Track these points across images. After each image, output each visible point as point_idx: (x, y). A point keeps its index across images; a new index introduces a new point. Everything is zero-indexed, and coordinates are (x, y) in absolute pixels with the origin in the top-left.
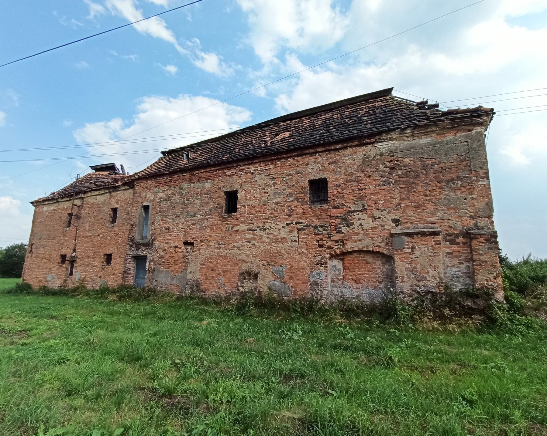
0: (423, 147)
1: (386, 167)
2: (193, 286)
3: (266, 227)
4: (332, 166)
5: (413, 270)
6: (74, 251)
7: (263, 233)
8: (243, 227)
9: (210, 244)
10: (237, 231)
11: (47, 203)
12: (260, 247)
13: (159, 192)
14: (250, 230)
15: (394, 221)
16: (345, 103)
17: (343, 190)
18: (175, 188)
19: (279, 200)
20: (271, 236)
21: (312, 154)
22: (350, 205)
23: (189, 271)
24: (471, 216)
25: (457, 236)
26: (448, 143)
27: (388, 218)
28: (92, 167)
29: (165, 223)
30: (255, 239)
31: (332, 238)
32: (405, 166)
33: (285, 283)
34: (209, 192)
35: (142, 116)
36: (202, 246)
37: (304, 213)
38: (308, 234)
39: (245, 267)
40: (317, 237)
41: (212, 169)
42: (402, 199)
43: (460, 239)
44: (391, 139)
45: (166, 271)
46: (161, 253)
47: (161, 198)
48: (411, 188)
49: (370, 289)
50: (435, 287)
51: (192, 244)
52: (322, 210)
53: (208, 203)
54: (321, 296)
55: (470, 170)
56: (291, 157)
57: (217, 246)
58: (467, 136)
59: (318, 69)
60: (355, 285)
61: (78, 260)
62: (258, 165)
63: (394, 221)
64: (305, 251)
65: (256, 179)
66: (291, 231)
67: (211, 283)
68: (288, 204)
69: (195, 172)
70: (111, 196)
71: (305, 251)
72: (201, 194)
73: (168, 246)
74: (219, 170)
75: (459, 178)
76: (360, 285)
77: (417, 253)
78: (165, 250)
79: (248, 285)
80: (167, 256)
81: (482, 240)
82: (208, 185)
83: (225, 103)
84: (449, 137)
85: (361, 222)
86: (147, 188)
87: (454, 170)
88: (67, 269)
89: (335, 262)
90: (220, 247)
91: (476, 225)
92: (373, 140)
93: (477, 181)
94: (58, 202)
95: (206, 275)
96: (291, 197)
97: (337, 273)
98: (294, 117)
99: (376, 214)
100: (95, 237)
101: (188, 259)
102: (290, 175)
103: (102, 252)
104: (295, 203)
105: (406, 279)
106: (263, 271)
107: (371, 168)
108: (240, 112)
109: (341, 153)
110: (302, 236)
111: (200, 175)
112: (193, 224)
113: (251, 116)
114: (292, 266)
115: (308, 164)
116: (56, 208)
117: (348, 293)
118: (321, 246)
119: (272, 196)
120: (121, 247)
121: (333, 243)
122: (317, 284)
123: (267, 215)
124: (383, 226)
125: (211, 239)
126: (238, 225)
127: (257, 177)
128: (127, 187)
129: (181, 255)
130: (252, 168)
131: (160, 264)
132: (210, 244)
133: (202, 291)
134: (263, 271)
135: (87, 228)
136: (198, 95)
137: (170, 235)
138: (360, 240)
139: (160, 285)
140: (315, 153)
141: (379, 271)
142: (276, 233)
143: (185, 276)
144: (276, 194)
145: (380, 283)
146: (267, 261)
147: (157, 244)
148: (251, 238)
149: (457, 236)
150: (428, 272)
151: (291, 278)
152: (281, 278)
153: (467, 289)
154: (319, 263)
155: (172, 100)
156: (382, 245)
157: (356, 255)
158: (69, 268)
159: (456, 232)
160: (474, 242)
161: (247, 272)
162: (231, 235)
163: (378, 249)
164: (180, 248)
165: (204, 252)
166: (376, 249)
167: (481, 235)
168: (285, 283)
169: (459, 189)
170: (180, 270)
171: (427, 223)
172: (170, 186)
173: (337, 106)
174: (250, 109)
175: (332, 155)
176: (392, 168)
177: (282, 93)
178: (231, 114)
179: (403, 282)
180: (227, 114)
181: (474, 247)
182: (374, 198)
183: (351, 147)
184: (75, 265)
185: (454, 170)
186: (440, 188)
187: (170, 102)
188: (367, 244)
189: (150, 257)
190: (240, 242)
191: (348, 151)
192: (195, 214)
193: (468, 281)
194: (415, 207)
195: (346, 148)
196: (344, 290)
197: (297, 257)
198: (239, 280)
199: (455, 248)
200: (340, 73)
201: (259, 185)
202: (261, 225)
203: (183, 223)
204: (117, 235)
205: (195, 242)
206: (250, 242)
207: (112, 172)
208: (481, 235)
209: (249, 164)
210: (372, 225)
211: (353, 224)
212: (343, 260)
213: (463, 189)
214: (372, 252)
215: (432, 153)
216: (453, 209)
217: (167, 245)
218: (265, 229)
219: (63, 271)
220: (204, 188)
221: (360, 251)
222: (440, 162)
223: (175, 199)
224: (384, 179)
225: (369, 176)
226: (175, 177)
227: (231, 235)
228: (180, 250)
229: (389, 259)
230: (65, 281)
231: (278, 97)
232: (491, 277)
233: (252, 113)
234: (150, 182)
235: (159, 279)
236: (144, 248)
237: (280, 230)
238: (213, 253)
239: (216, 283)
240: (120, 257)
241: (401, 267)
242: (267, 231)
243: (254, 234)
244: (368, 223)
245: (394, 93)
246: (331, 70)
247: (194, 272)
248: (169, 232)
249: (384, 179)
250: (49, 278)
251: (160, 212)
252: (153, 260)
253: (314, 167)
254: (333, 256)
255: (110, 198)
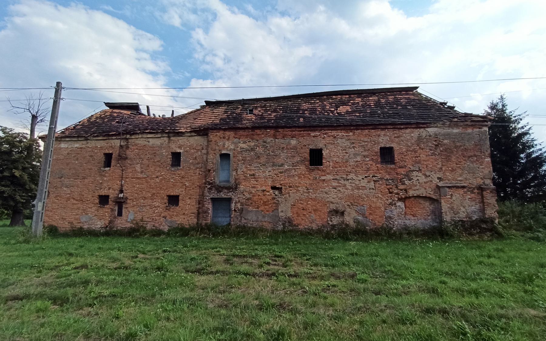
0: (456, 134)
1: (433, 144)
2: (286, 222)
3: (348, 178)
4: (397, 139)
5: (452, 208)
6: (121, 191)
7: (346, 182)
8: (329, 177)
9: (299, 189)
10: (324, 180)
11: (67, 139)
12: (345, 192)
13: (240, 143)
14: (336, 179)
15: (438, 178)
16: (385, 91)
17: (405, 156)
18: (257, 140)
19: (359, 159)
20: (354, 185)
21: (382, 129)
22: (411, 167)
23: (280, 210)
24: (481, 178)
25: (474, 189)
26: (469, 134)
27: (434, 177)
28: (107, 104)
29: (250, 170)
30: (340, 187)
31: (399, 188)
32: (445, 145)
33: (366, 217)
34: (295, 148)
35: (18, 20)
36: (291, 190)
37: (378, 170)
38: (381, 184)
39: (333, 207)
40: (388, 187)
41: (298, 129)
42: (442, 165)
43: (476, 191)
44: (436, 127)
45: (256, 211)
46: (248, 196)
47: (243, 148)
48: (448, 159)
49: (423, 220)
50: (464, 218)
51: (280, 189)
52: (391, 168)
53: (294, 156)
54: (394, 225)
55: (481, 152)
56: (366, 129)
57: (306, 191)
58: (479, 131)
59: (236, 10)
60: (413, 218)
61: (128, 201)
62: (339, 131)
63: (438, 178)
64: (380, 196)
65: (338, 141)
66: (369, 182)
67: (303, 220)
68: (366, 163)
69: (280, 130)
70: (169, 140)
71: (380, 196)
72: (287, 149)
73: (255, 189)
74: (304, 131)
75: (475, 156)
76: (416, 218)
77: (454, 198)
78: (251, 193)
79: (336, 220)
80: (255, 198)
81: (488, 191)
82: (294, 142)
83: (132, 27)
84: (470, 130)
85: (418, 178)
86: (224, 138)
87: (472, 151)
88: (112, 210)
89: (399, 204)
90: (309, 192)
91: (484, 183)
92: (425, 126)
93: (485, 158)
94: (87, 139)
95: (297, 213)
96: (367, 157)
97: (401, 210)
98: (344, 93)
99: (428, 174)
100: (153, 178)
101: (278, 201)
102: (366, 142)
103: (164, 194)
104: (371, 162)
105: (448, 213)
106: (348, 210)
107: (423, 144)
108: (150, 39)
109: (403, 131)
110: (377, 185)
111: (284, 132)
112: (281, 173)
113: (162, 46)
114: (371, 206)
115: (379, 136)
116: (84, 146)
117: (408, 222)
118: (390, 193)
119: (352, 156)
120: (190, 190)
121: (399, 191)
122: (390, 217)
123: (349, 169)
124: (431, 181)
125: (300, 185)
126: (325, 175)
127: (339, 141)
128: (193, 134)
129: (270, 198)
130: (334, 133)
131: (248, 205)
132: (299, 189)
133: (295, 225)
134: (348, 210)
135: (139, 170)
136: (98, 9)
137: (257, 181)
138: (417, 190)
139: (251, 222)
140: (385, 129)
141: (428, 209)
142: (357, 183)
143: (277, 215)
144: (355, 155)
145: (429, 216)
146: (351, 203)
147: (242, 188)
148: (337, 186)
149: (474, 189)
150: (460, 209)
151: (370, 214)
152: (363, 215)
153: (480, 218)
154: (391, 204)
155: (61, 8)
156: (432, 193)
157: (413, 199)
158: (116, 208)
159: (473, 186)
160: (484, 193)
161: (334, 210)
162: (319, 183)
163: (429, 195)
164: (268, 192)
165: (294, 196)
166: (428, 195)
167: (488, 189)
168: (366, 217)
169: (475, 162)
170: (271, 209)
171: (458, 181)
172: (253, 139)
173: (379, 91)
174: (162, 37)
175: (397, 131)
176: (436, 145)
177: (199, 27)
178: (139, 39)
179: (446, 215)
180: (135, 39)
181: (485, 195)
182: (425, 163)
183: (410, 128)
184: (124, 206)
185: (472, 151)
186: (465, 160)
187: (59, 10)
188: (422, 192)
189: (235, 199)
190: (327, 188)
191: (408, 131)
192: (282, 165)
193: (481, 214)
194: (450, 170)
195: (406, 128)
196: (406, 221)
197: (375, 200)
198: (328, 217)
199: (473, 195)
200: (256, 19)
201: (341, 147)
202: (345, 176)
203: (270, 171)
204: (183, 177)
205: (283, 187)
206: (335, 189)
207: (135, 112)
208: (488, 189)
209: (332, 130)
210: (425, 180)
211: (412, 179)
212: (404, 202)
213: (477, 163)
214: (425, 198)
215: (460, 139)
216: (472, 173)
217: (253, 189)
218: (348, 180)
219: (106, 212)
220: (289, 144)
221: (419, 197)
222: (464, 145)
223: (260, 150)
224: (432, 152)
225: (422, 149)
226: (258, 131)
227: (319, 183)
228: (268, 194)
229: (435, 201)
230: (110, 222)
231: (194, 30)
232: (493, 211)
233: (162, 43)
234: (228, 133)
235: (249, 218)
236: (226, 191)
237: (360, 180)
238: (302, 196)
239: (307, 218)
240: (190, 198)
241: (445, 207)
242: (350, 181)
243: (339, 183)
244: (423, 179)
245: (419, 90)
246: (249, 14)
247: (285, 210)
248: (255, 178)
249: (432, 152)
250: (84, 219)
251: (242, 160)
252: (239, 201)
253: (384, 138)
254: (400, 199)
255: (169, 142)
